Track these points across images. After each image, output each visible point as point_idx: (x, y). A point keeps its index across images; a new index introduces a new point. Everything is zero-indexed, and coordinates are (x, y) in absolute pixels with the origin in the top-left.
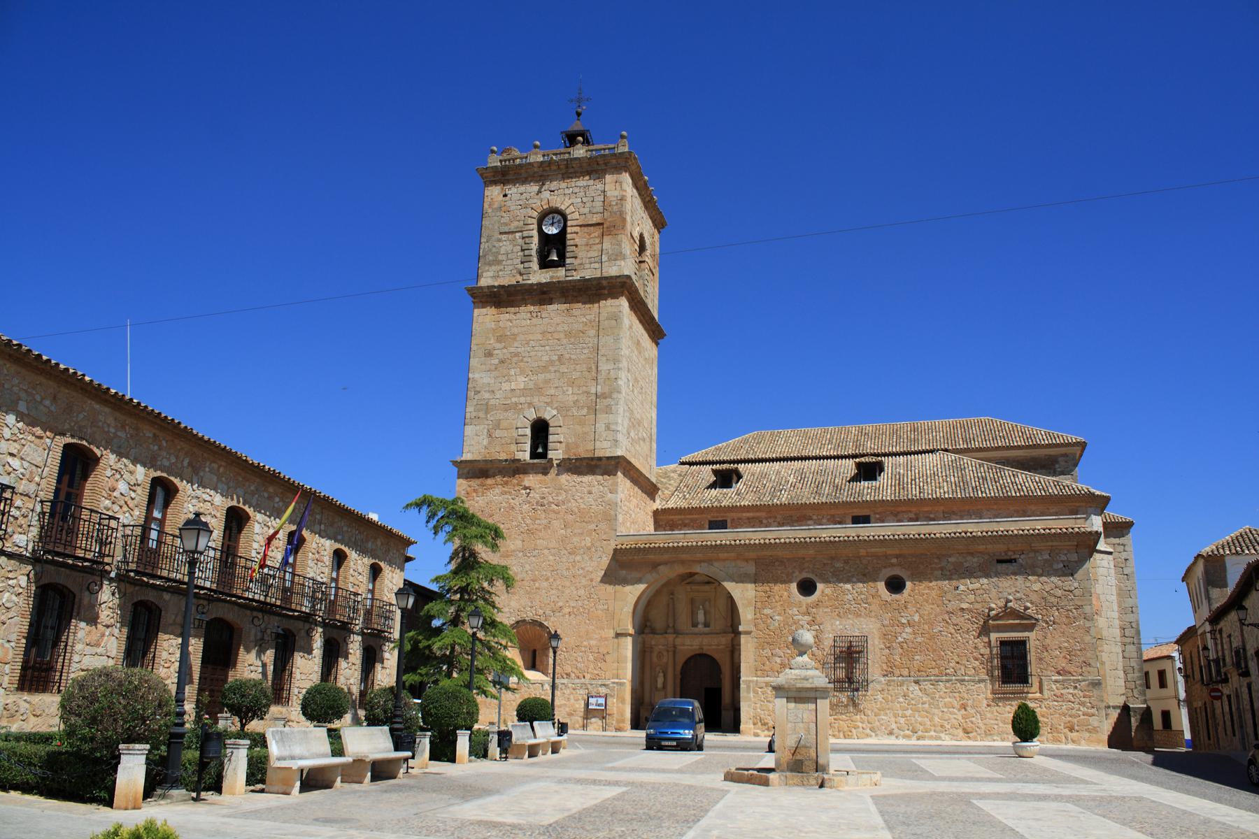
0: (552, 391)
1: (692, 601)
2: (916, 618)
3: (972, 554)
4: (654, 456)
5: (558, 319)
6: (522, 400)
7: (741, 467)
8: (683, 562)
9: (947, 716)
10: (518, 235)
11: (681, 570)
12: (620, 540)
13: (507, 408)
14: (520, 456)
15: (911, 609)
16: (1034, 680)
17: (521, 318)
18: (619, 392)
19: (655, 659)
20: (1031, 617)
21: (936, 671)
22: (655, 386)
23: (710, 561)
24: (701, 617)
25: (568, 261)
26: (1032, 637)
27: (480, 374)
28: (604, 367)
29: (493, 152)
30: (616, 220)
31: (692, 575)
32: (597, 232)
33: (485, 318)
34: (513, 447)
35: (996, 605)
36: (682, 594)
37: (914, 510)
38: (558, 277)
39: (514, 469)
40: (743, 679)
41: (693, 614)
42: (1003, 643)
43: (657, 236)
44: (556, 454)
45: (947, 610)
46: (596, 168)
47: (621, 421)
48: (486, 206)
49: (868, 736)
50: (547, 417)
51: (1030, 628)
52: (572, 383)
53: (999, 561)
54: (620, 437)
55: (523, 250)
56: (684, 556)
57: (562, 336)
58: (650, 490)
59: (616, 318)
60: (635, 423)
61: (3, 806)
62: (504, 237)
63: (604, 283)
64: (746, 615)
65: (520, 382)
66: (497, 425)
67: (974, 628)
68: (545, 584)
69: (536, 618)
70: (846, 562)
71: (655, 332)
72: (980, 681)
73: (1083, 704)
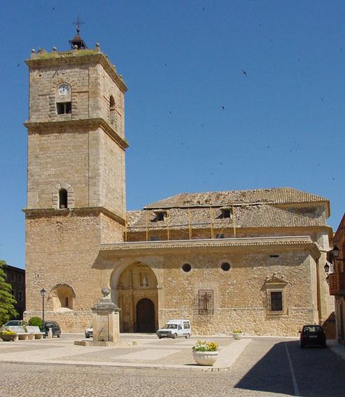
0: (68, 176)
1: (140, 274)
2: (235, 282)
3: (259, 253)
4: (125, 206)
5: (69, 140)
6: (54, 179)
7: (168, 211)
8: (131, 256)
9: (248, 325)
10: (48, 96)
11: (130, 261)
12: (102, 247)
13: (47, 183)
14: (54, 207)
15: (233, 278)
16: (285, 309)
17: (51, 139)
18: (99, 176)
19: (124, 302)
20: (284, 282)
21: (243, 305)
22: (124, 171)
23: (144, 256)
24: (144, 282)
25: (72, 110)
26: (285, 291)
27: (34, 168)
28: (92, 163)
29: (33, 52)
30: (101, 90)
31: (139, 262)
32: (86, 95)
33: (35, 139)
34: (51, 203)
35: (269, 277)
36: (136, 271)
37: (244, 232)
38: (69, 121)
39: (49, 214)
40: (159, 309)
41: (141, 281)
42: (272, 293)
43: (122, 96)
44: (71, 206)
45: (248, 279)
46: (85, 63)
47: (102, 190)
48: (31, 80)
49: (214, 334)
50: (66, 188)
51: (283, 286)
52: (77, 172)
53: (271, 256)
54: (101, 198)
55: (50, 104)
56: (131, 254)
57: (71, 148)
58: (122, 222)
59: (97, 139)
60: (110, 190)
61: (3, 355)
62: (41, 97)
63: (90, 122)
64: (160, 281)
65: (53, 171)
66: (43, 192)
67: (260, 287)
68: (69, 267)
69: (66, 283)
70: (204, 256)
71: (123, 145)
72: (262, 310)
73: (305, 319)
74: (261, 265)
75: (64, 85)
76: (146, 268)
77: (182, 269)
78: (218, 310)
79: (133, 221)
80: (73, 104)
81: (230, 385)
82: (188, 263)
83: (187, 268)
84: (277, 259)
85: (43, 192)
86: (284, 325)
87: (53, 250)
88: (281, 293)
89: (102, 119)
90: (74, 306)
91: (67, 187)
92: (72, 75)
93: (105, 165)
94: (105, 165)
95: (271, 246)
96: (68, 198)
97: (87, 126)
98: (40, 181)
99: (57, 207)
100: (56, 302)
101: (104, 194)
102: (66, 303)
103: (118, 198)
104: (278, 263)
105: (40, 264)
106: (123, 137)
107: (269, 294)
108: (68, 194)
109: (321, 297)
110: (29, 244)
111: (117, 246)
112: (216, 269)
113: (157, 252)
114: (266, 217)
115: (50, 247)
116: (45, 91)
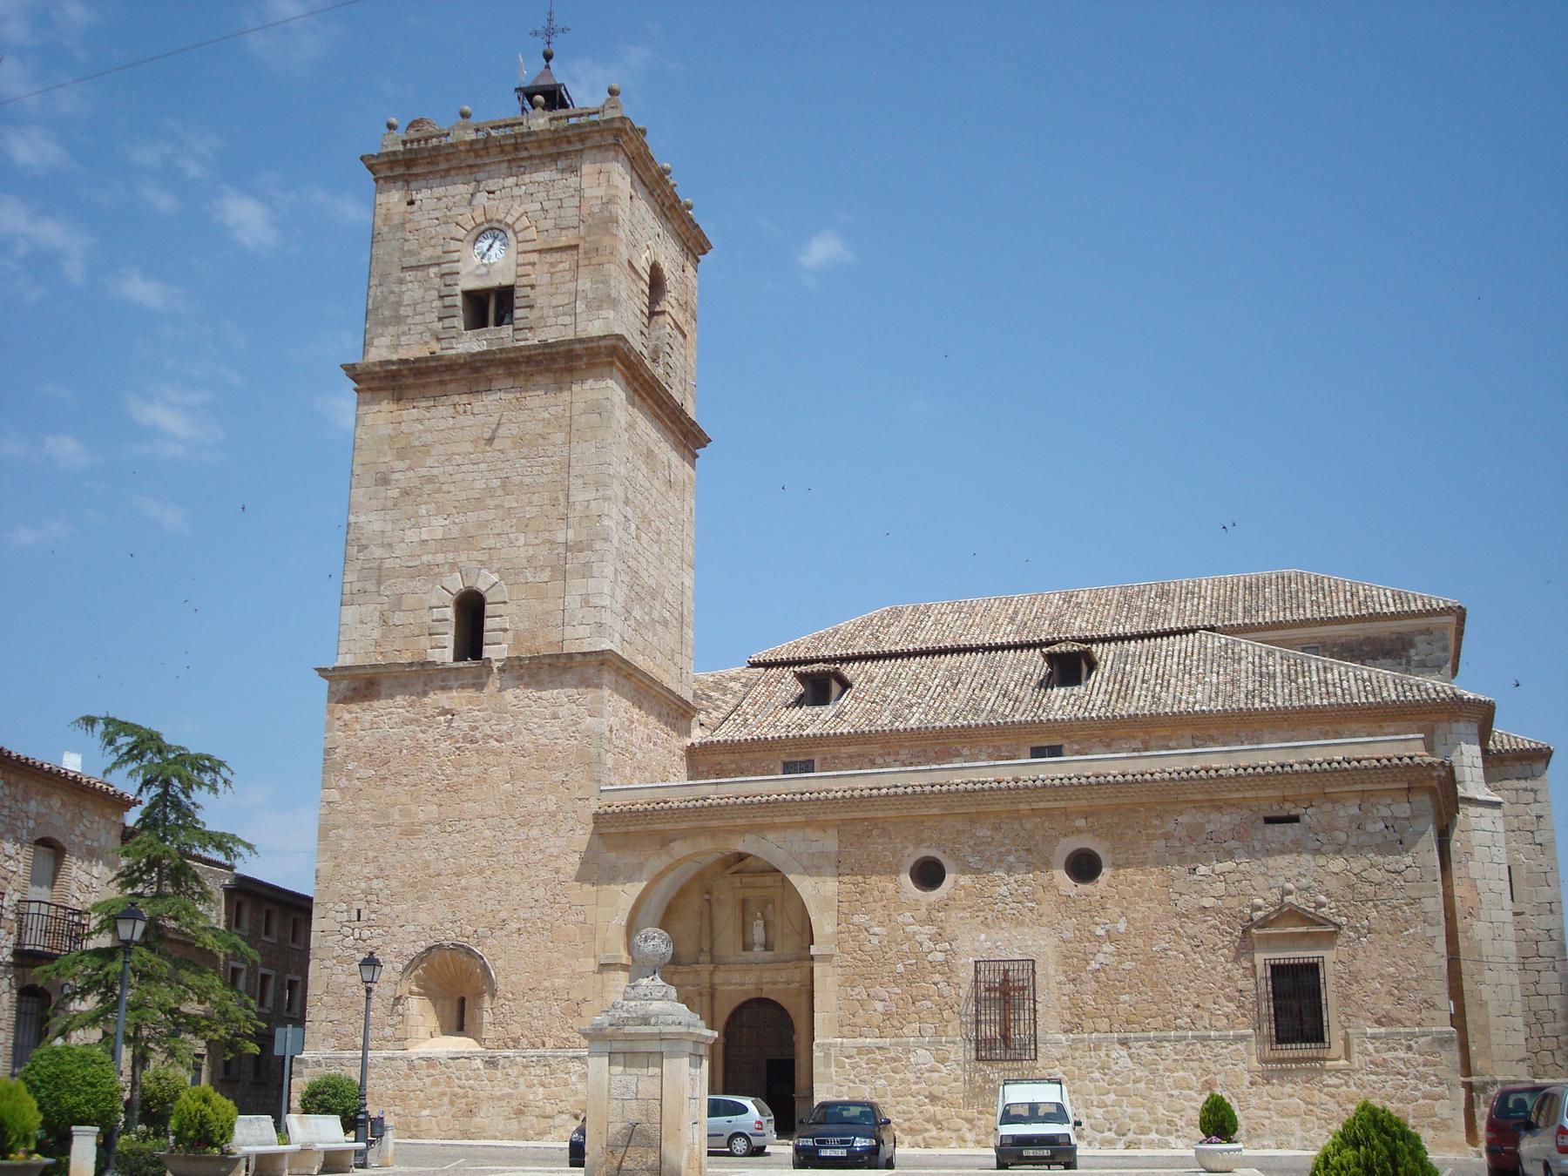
0: (491, 542)
1: (744, 904)
2: (1122, 926)
6: (440, 558)
7: (849, 671)
10: (433, 270)
11: (708, 849)
13: (414, 572)
16: (1334, 1033)
24: (758, 934)
25: (518, 313)
26: (1331, 961)
31: (741, 857)
32: (566, 261)
36: (727, 894)
39: (420, 677)
41: (745, 928)
42: (1278, 971)
48: (379, 221)
50: (482, 586)
51: (1329, 939)
52: (524, 526)
53: (1269, 820)
55: (441, 297)
58: (678, 712)
59: (599, 409)
60: (641, 594)
62: (409, 276)
64: (824, 926)
65: (436, 528)
66: (397, 604)
68: (477, 881)
69: (462, 940)
72: (1239, 1039)
73: (1422, 1077)
74: (1230, 855)
75: (493, 229)
76: (768, 880)
77: (906, 879)
78: (1057, 1043)
79: (717, 708)
80: (518, 293)
82: (934, 853)
83: (929, 874)
84: (1291, 830)
86: (1332, 1105)
87: (422, 817)
88: (1312, 969)
89: (621, 338)
90: (489, 1033)
91: (483, 582)
92: (525, 197)
93: (627, 502)
94: (627, 502)
95: (1264, 777)
96: (489, 623)
97: (564, 362)
98: (388, 564)
99: (446, 655)
100: (421, 1014)
101: (618, 608)
102: (459, 1021)
103: (665, 623)
104: (1297, 847)
105: (369, 870)
107: (1263, 972)
108: (489, 609)
109: (1467, 985)
110: (335, 795)
111: (661, 794)
112: (1044, 878)
113: (811, 813)
114: (1188, 679)
115: (413, 807)
116: (426, 254)
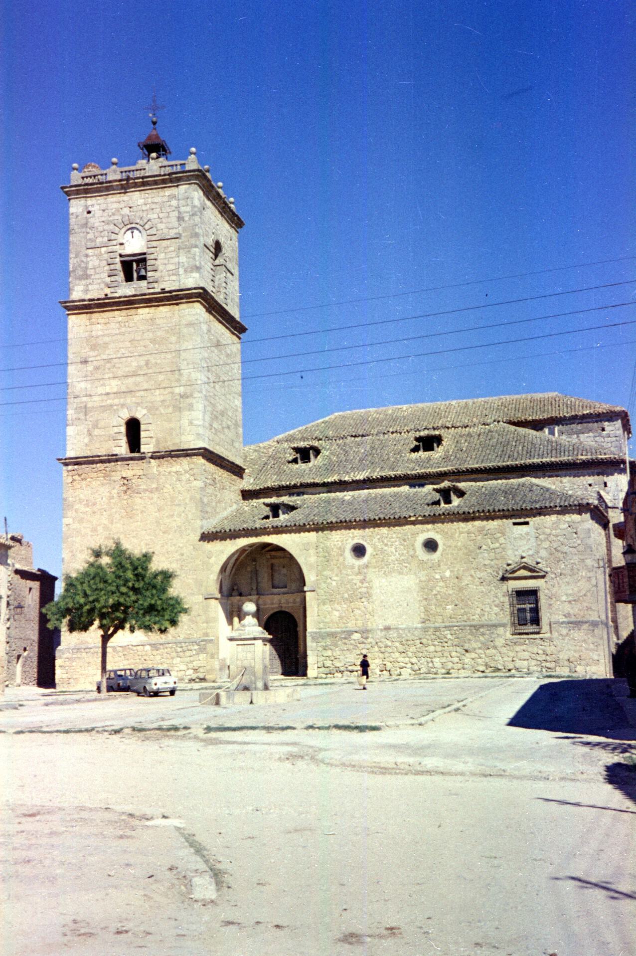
2: (448, 574)
10: (103, 249)
44: (146, 447)
58: (237, 471)
62: (90, 251)
65: (114, 385)
71: (237, 328)
81: (106, 528)
85: (95, 426)
96: (143, 434)
106: (237, 317)
108: (142, 427)
